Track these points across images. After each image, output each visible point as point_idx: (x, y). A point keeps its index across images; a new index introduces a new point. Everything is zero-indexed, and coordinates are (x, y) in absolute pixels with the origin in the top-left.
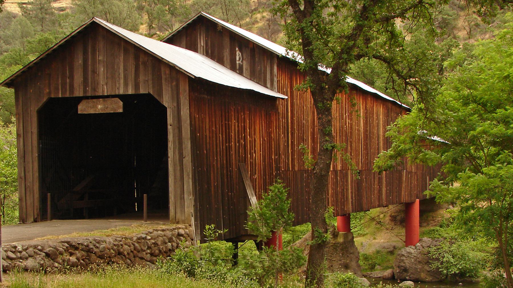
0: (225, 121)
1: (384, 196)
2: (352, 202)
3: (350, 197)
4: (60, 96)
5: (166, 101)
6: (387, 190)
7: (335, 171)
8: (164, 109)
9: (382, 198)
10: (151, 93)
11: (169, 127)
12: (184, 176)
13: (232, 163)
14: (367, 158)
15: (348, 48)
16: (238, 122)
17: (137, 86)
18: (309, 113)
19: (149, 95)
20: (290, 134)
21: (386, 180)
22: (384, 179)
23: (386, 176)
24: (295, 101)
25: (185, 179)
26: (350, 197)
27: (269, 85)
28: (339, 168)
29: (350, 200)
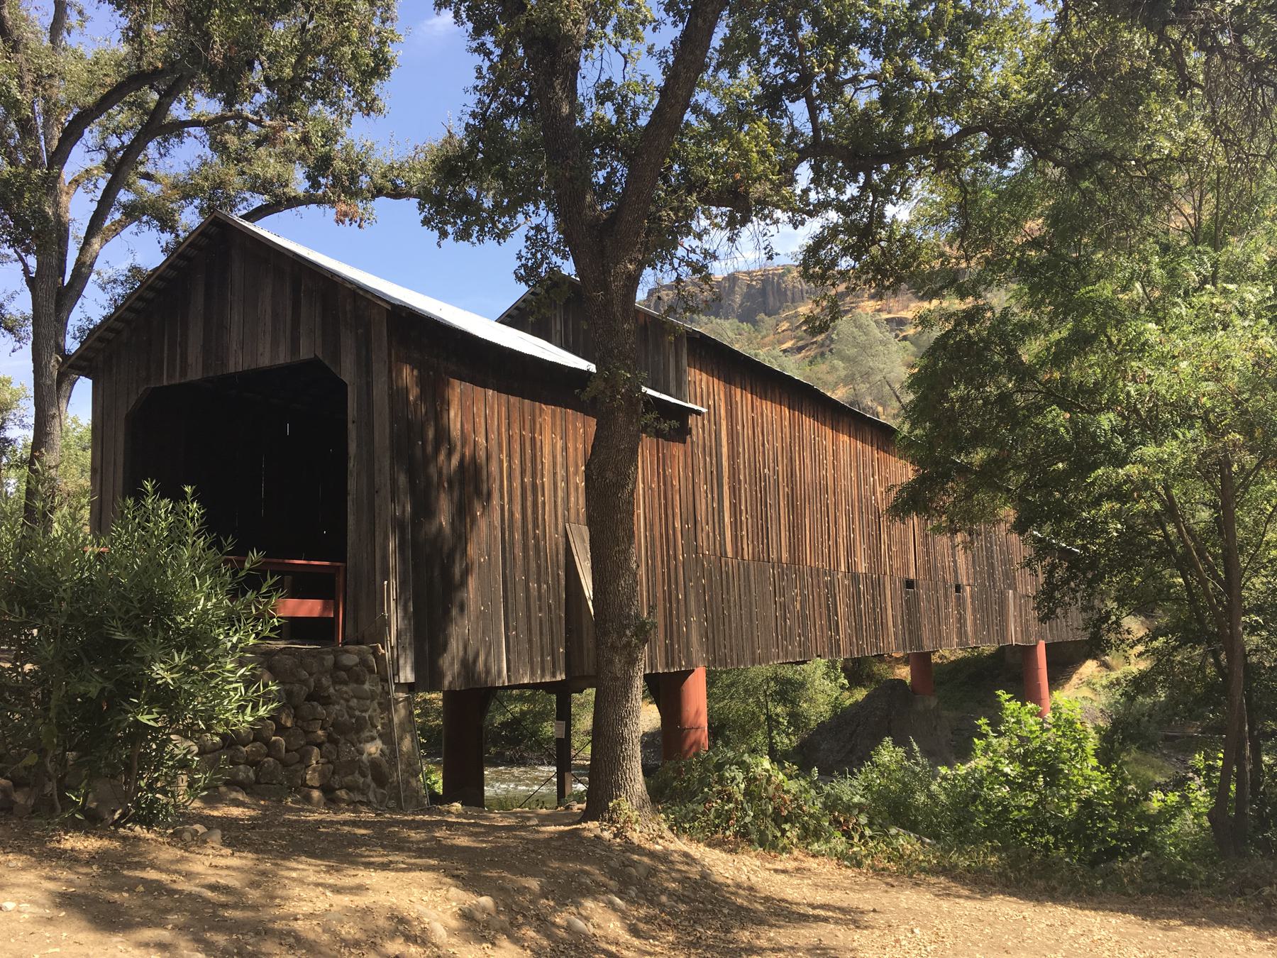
0: (522, 427)
1: (969, 628)
2: (895, 634)
3: (890, 624)
4: (165, 383)
5: (348, 372)
6: (975, 619)
7: (855, 578)
8: (344, 386)
9: (966, 631)
10: (320, 356)
11: (350, 425)
12: (377, 533)
13: (544, 519)
14: (929, 561)
15: (1049, 619)
16: (565, 437)
17: (295, 348)
18: (780, 458)
19: (316, 358)
20: (726, 488)
21: (972, 603)
22: (969, 600)
23: (972, 597)
24: (739, 428)
25: (377, 539)
26: (890, 624)
27: (673, 389)
28: (862, 568)
29: (892, 630)
